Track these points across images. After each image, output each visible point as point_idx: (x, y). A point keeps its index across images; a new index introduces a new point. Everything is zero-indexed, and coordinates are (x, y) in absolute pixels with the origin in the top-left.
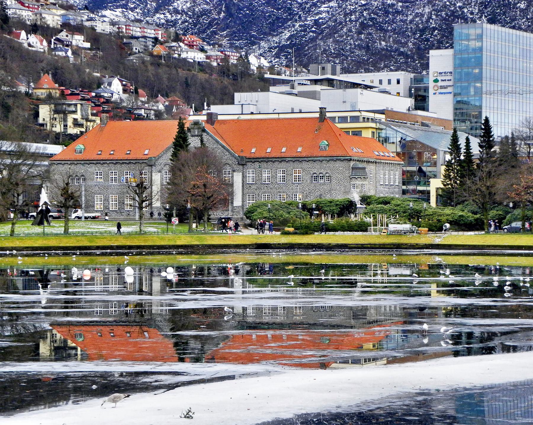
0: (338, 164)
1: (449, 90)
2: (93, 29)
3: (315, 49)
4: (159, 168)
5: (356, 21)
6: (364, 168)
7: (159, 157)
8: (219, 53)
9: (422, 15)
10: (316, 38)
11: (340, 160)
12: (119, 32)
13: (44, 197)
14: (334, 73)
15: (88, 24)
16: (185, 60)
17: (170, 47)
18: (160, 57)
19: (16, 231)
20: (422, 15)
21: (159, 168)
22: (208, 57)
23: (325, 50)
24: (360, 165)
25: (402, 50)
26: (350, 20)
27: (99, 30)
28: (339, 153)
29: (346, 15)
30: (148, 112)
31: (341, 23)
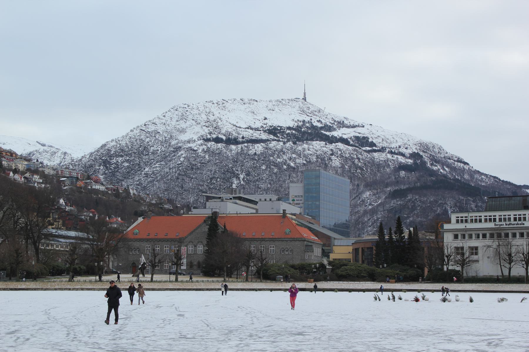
0: (297, 243)
1: (302, 205)
2: (43, 172)
3: (153, 187)
4: (185, 244)
5: (176, 172)
6: (312, 246)
7: (186, 237)
8: (112, 187)
9: (211, 171)
10: (154, 180)
11: (299, 240)
12: (57, 174)
13: (143, 259)
14: (240, 193)
15: (40, 169)
16: (94, 189)
17: (86, 183)
18: (81, 188)
19: (154, 279)
20: (211, 171)
21: (185, 244)
22: (106, 188)
23: (159, 187)
24: (310, 244)
25: (201, 188)
26: (173, 172)
27: (46, 173)
28: (297, 236)
29: (170, 169)
30: (86, 217)
31: (167, 173)
